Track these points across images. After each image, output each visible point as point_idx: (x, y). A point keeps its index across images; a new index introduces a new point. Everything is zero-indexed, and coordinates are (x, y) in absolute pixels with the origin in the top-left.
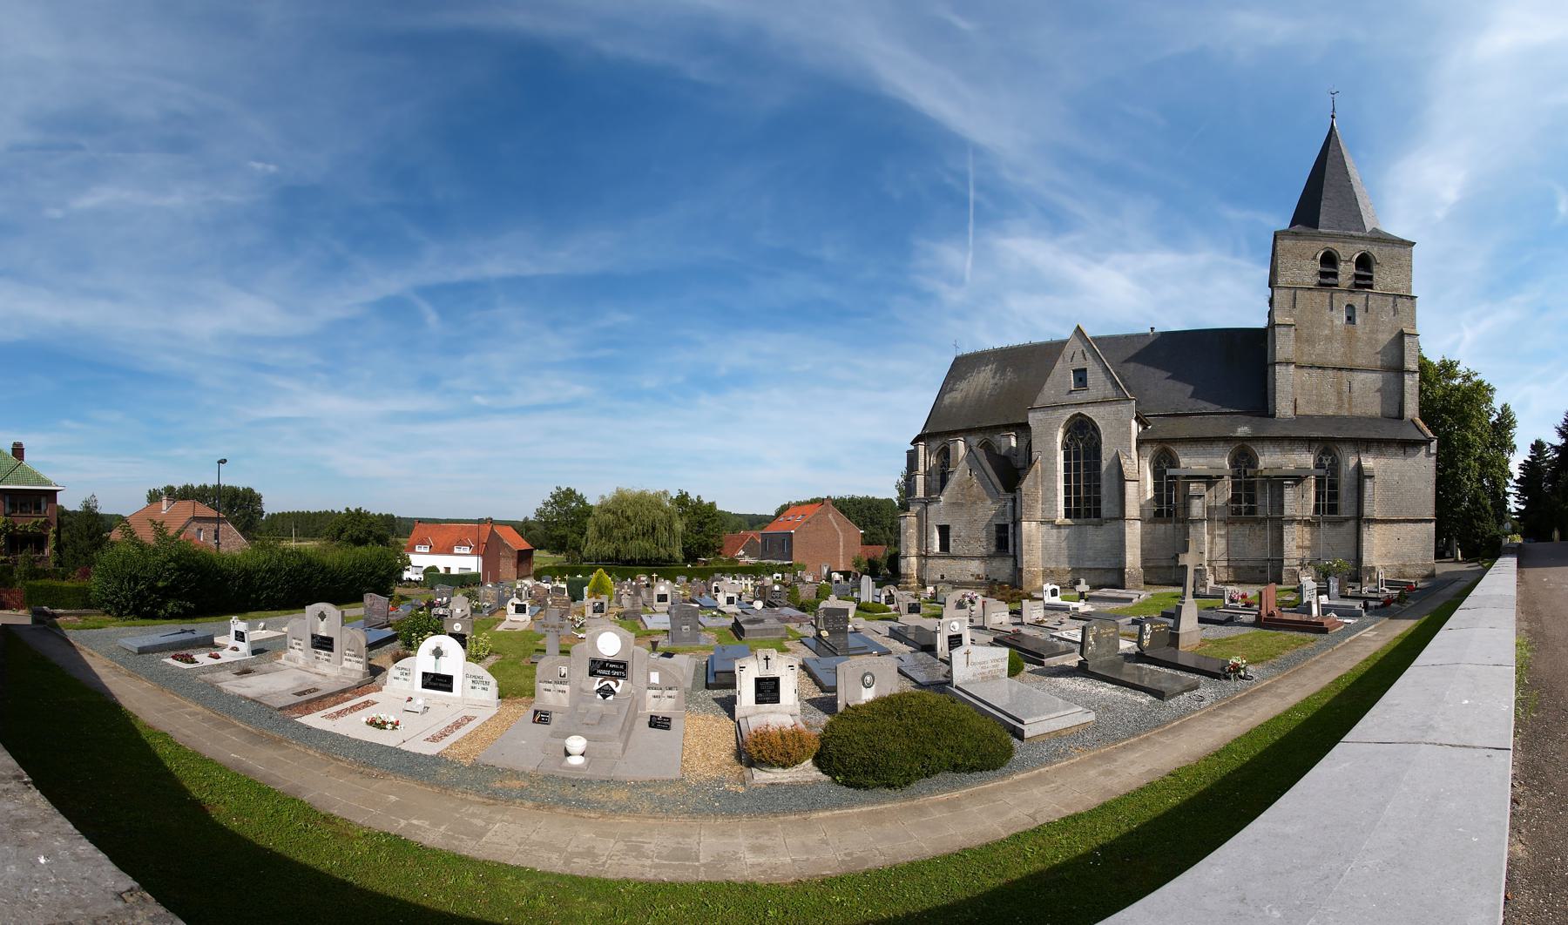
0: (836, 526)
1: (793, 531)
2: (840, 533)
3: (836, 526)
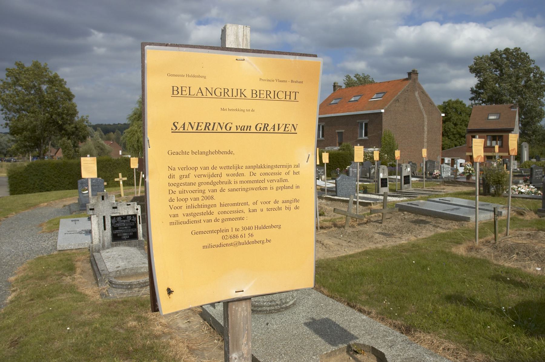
0: (422, 107)
1: (383, 111)
2: (425, 116)
3: (422, 107)
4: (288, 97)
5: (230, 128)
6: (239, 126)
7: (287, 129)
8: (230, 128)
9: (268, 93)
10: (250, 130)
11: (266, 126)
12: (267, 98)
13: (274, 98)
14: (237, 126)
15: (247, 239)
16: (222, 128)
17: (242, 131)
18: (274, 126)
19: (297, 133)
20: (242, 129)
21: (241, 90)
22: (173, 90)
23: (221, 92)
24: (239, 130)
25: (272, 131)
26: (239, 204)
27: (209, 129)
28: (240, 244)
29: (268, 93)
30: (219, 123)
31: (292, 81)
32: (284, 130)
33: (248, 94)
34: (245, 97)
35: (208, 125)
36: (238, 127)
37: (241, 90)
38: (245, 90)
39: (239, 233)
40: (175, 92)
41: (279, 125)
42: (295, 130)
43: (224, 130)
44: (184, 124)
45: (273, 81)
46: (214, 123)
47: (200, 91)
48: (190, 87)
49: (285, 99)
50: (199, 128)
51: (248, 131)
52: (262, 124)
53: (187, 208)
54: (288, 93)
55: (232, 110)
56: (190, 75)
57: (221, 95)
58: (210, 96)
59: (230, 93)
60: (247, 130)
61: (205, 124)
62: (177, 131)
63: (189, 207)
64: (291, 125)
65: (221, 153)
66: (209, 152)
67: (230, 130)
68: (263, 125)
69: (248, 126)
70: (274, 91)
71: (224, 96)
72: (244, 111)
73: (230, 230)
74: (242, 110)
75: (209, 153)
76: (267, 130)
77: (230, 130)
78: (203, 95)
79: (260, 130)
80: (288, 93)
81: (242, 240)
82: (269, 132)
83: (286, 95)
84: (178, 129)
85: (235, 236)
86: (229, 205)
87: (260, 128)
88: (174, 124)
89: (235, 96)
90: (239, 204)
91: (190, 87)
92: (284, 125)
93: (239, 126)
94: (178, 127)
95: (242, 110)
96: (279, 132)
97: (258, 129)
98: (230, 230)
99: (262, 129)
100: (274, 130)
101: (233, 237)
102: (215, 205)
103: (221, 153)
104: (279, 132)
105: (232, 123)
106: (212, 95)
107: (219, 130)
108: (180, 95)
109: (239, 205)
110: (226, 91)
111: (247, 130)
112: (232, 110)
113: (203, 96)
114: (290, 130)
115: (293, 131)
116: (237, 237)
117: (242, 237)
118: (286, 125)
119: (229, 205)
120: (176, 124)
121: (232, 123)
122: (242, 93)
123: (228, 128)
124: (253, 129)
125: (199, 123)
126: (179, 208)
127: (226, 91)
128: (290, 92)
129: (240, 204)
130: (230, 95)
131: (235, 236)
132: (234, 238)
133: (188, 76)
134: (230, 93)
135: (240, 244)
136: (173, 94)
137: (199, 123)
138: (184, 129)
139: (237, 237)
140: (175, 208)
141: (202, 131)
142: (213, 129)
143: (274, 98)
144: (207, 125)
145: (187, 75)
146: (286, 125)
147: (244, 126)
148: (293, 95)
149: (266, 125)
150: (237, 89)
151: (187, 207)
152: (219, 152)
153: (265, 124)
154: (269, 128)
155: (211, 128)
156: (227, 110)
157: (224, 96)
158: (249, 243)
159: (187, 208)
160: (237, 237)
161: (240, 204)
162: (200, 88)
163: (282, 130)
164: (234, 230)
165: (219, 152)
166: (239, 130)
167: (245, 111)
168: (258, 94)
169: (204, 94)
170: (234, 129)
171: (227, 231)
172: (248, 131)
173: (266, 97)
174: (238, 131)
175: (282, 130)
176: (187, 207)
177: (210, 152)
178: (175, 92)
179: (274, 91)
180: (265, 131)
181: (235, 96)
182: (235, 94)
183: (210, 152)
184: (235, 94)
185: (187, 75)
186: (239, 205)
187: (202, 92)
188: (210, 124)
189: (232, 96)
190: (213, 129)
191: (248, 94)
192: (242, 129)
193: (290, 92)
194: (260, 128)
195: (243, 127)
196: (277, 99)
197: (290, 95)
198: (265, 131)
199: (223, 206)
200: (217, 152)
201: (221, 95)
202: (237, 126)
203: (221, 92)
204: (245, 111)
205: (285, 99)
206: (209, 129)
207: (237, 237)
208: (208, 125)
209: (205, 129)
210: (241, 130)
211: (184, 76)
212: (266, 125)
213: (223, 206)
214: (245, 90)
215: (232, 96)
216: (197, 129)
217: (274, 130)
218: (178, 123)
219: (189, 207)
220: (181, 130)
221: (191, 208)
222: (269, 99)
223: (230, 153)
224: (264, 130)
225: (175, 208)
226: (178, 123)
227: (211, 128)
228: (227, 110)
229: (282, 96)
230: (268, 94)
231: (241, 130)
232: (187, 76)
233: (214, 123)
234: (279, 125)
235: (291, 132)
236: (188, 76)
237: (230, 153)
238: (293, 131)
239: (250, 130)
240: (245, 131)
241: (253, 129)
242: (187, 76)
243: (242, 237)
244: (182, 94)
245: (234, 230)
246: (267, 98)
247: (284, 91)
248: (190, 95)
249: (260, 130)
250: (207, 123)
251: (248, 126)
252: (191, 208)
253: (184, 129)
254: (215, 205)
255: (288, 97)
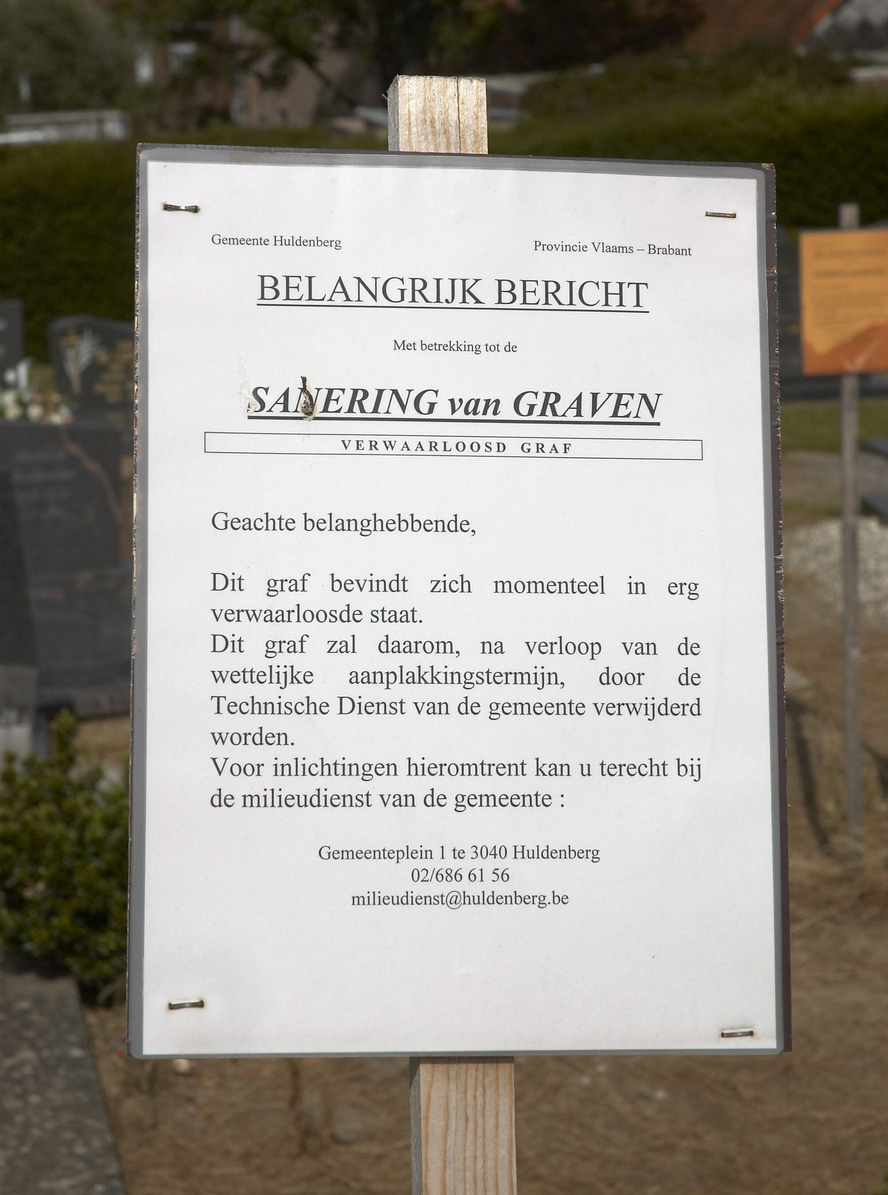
4: (614, 300)
5: (432, 406)
6: (461, 401)
7: (622, 411)
8: (432, 406)
9: (552, 287)
10: (495, 413)
11: (551, 400)
12: (547, 303)
13: (571, 303)
14: (452, 401)
15: (489, 886)
16: (403, 408)
17: (471, 417)
18: (579, 399)
19: (658, 424)
20: (470, 409)
21: (464, 281)
22: (263, 287)
23: (402, 291)
24: (460, 414)
25: (571, 415)
26: (486, 768)
27: (362, 410)
28: (467, 899)
29: (552, 287)
30: (395, 392)
31: (653, 249)
32: (615, 414)
33: (487, 293)
34: (478, 301)
35: (360, 395)
36: (457, 404)
37: (464, 281)
38: (477, 280)
39: (466, 865)
40: (270, 293)
41: (595, 396)
42: (652, 412)
43: (411, 412)
44: (286, 394)
45: (584, 249)
46: (380, 392)
47: (339, 289)
48: (310, 278)
49: (607, 304)
50: (333, 406)
51: (490, 416)
52: (536, 394)
53: (279, 772)
54: (614, 288)
55: (436, 347)
56: (287, 237)
57: (403, 299)
58: (369, 300)
59: (430, 292)
60: (485, 413)
61: (349, 394)
62: (263, 413)
63: (286, 768)
64: (638, 398)
65: (423, 526)
66: (372, 523)
67: (431, 411)
68: (542, 397)
69: (488, 401)
70: (571, 283)
71: (413, 300)
72: (477, 350)
73: (437, 854)
74: (469, 348)
75: (371, 527)
76: (554, 413)
77: (431, 411)
78: (348, 299)
79: (530, 413)
80: (614, 288)
81: (474, 889)
82: (563, 419)
83: (607, 294)
84: (267, 408)
85: (453, 875)
86: (445, 769)
87: (532, 407)
88: (255, 392)
89: (447, 301)
90: (486, 768)
91: (310, 278)
92: (614, 398)
93: (461, 401)
94: (269, 400)
95: (469, 348)
96: (596, 418)
97: (524, 409)
98: (437, 854)
99: (538, 410)
100: (579, 414)
101: (445, 875)
102: (392, 768)
103: (423, 526)
104: (593, 419)
105: (436, 392)
106: (375, 297)
107: (396, 411)
108: (280, 300)
109: (486, 771)
110: (419, 285)
111: (485, 413)
112: (436, 347)
113: (348, 303)
114: (634, 414)
115: (645, 416)
116: (458, 877)
117: (472, 877)
118: (620, 396)
119: (445, 769)
120: (261, 393)
121: (436, 392)
122: (468, 291)
123: (424, 406)
124: (507, 411)
125: (330, 391)
126: (249, 770)
127: (419, 285)
128: (621, 284)
129: (493, 769)
130: (432, 297)
131: (453, 875)
132: (449, 878)
133: (280, 241)
134: (430, 292)
135: (467, 899)
136: (263, 298)
137: (330, 391)
138: (286, 409)
139: (458, 877)
140: (236, 770)
141: (341, 415)
142: (375, 410)
143: (571, 303)
144: (358, 397)
145: (278, 238)
146: (620, 396)
147: (477, 401)
148: (629, 294)
149: (552, 399)
150: (453, 281)
151: (279, 768)
152: (413, 524)
153: (548, 395)
154: (560, 408)
155: (369, 404)
156: (418, 346)
157: (413, 300)
158: (495, 900)
159: (279, 772)
160: (456, 876)
161: (493, 769)
162: (340, 280)
163: (605, 413)
164: (449, 854)
165: (413, 524)
166: (460, 414)
167: (483, 349)
168: (519, 291)
169: (353, 295)
170: (443, 410)
171: (427, 854)
172: (490, 416)
173: (543, 301)
174: (456, 416)
175: (605, 413)
176: (279, 768)
177: (379, 524)
178: (270, 293)
179: (571, 283)
180: (549, 416)
181: (447, 301)
182: (446, 294)
183: (379, 524)
184: (446, 294)
185: (278, 238)
186: (486, 771)
187: (345, 292)
188: (366, 394)
189: (438, 301)
190: (375, 410)
191: (487, 293)
192: (470, 409)
193: (621, 284)
194: (532, 407)
195: (473, 403)
196: (581, 306)
197: (621, 294)
198: (549, 416)
199: (420, 772)
200: (403, 524)
201: (403, 299)
202: (452, 401)
203: (402, 291)
204: (483, 349)
205: (607, 304)
206: (362, 410)
207: (456, 876)
208: (360, 395)
209: (350, 410)
210: (467, 413)
211: (265, 242)
212: (552, 399)
213: (420, 772)
214: (477, 280)
215: (438, 301)
216: (325, 410)
217: (579, 414)
218: (266, 390)
219: (286, 768)
220: (278, 410)
221: (293, 772)
222: (555, 305)
223: (459, 526)
224: (543, 413)
225: (236, 770)
226: (266, 390)
227: (369, 404)
228: (418, 346)
229: (593, 295)
230: (551, 290)
231: (467, 412)
232: (278, 243)
233: (380, 392)
234: (595, 396)
235: (637, 420)
236: (280, 241)
237: (459, 526)
238: (650, 419)
239: (495, 413)
240: (480, 416)
241: (507, 411)
242: (278, 243)
243: (472, 877)
244: (288, 298)
245: (449, 854)
246: (547, 303)
247: (601, 279)
248: (310, 299)
249: (530, 413)
250: (355, 392)
251: (488, 401)
252: (293, 772)
253: (286, 409)
254: (392, 768)
255: (614, 300)
